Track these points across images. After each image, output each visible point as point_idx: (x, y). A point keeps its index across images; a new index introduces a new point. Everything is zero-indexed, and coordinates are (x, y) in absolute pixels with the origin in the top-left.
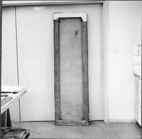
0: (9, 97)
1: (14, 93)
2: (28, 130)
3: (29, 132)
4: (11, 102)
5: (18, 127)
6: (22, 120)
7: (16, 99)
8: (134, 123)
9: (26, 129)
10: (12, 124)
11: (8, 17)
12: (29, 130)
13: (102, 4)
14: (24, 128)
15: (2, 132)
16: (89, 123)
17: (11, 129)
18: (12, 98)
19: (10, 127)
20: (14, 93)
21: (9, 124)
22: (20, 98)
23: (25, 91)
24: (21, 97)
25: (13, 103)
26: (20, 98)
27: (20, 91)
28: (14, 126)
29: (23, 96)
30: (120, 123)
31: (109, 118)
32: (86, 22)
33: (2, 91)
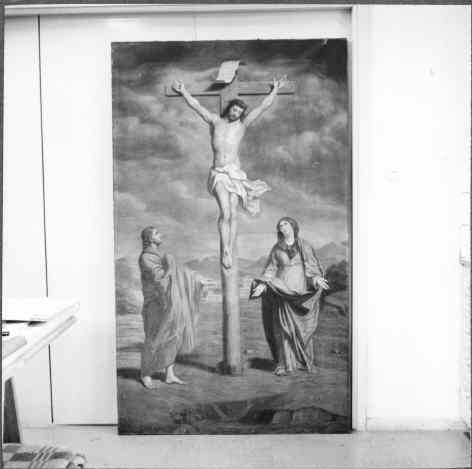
0: (13, 339)
1: (32, 323)
2: (78, 455)
3: (80, 461)
4: (20, 357)
5: (43, 445)
6: (60, 419)
7: (36, 344)
8: (456, 433)
9: (74, 453)
10: (24, 434)
11: (19, 44)
12: (83, 457)
13: (350, 10)
14: (62, 448)
15: (308, 307)
16: (128, 214)
17: (19, 452)
18: (26, 343)
19: (18, 445)
20: (32, 323)
21: (13, 436)
22: (52, 340)
23: (71, 318)
24: (56, 337)
25: (26, 360)
26: (52, 340)
27: (52, 319)
28: (29, 441)
29: (64, 335)
30: (408, 432)
31: (369, 416)
32: (221, 363)
33: (5, 317)
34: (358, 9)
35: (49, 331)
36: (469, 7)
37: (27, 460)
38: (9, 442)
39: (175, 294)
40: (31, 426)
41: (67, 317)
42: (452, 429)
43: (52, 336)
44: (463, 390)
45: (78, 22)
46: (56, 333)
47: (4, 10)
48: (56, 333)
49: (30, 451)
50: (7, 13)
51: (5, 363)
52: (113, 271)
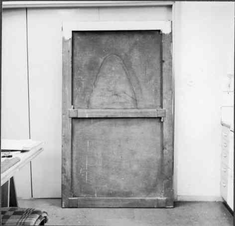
0: (14, 158)
1: (23, 151)
3: (45, 215)
8: (219, 202)
9: (42, 211)
11: (11, 23)
12: (46, 213)
13: (171, 6)
14: (37, 209)
20: (23, 151)
21: (14, 203)
23: (41, 149)
28: (22, 205)
34: (176, 5)
35: (30, 155)
36: (234, 2)
37: (19, 215)
38: (12, 206)
39: (67, 158)
40: (23, 198)
41: (40, 148)
42: (217, 201)
43: (31, 158)
44: (222, 183)
45: (146, 9)
46: (34, 156)
47: (1, 4)
48: (34, 156)
49: (21, 210)
50: (3, 7)
51: (1, 175)
52: (173, 56)
